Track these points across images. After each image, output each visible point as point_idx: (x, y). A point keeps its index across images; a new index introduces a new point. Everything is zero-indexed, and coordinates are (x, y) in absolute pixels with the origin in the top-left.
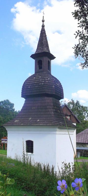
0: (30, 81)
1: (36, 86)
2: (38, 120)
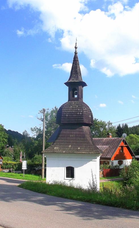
0: (67, 110)
1: (74, 115)
2: (79, 148)
